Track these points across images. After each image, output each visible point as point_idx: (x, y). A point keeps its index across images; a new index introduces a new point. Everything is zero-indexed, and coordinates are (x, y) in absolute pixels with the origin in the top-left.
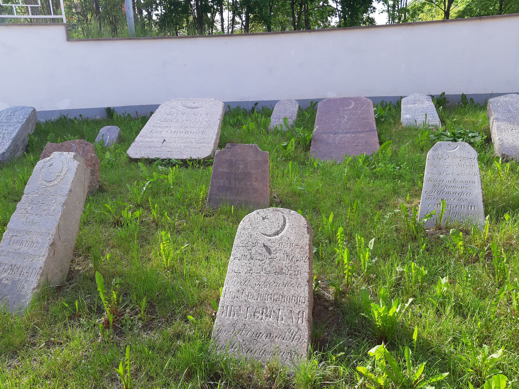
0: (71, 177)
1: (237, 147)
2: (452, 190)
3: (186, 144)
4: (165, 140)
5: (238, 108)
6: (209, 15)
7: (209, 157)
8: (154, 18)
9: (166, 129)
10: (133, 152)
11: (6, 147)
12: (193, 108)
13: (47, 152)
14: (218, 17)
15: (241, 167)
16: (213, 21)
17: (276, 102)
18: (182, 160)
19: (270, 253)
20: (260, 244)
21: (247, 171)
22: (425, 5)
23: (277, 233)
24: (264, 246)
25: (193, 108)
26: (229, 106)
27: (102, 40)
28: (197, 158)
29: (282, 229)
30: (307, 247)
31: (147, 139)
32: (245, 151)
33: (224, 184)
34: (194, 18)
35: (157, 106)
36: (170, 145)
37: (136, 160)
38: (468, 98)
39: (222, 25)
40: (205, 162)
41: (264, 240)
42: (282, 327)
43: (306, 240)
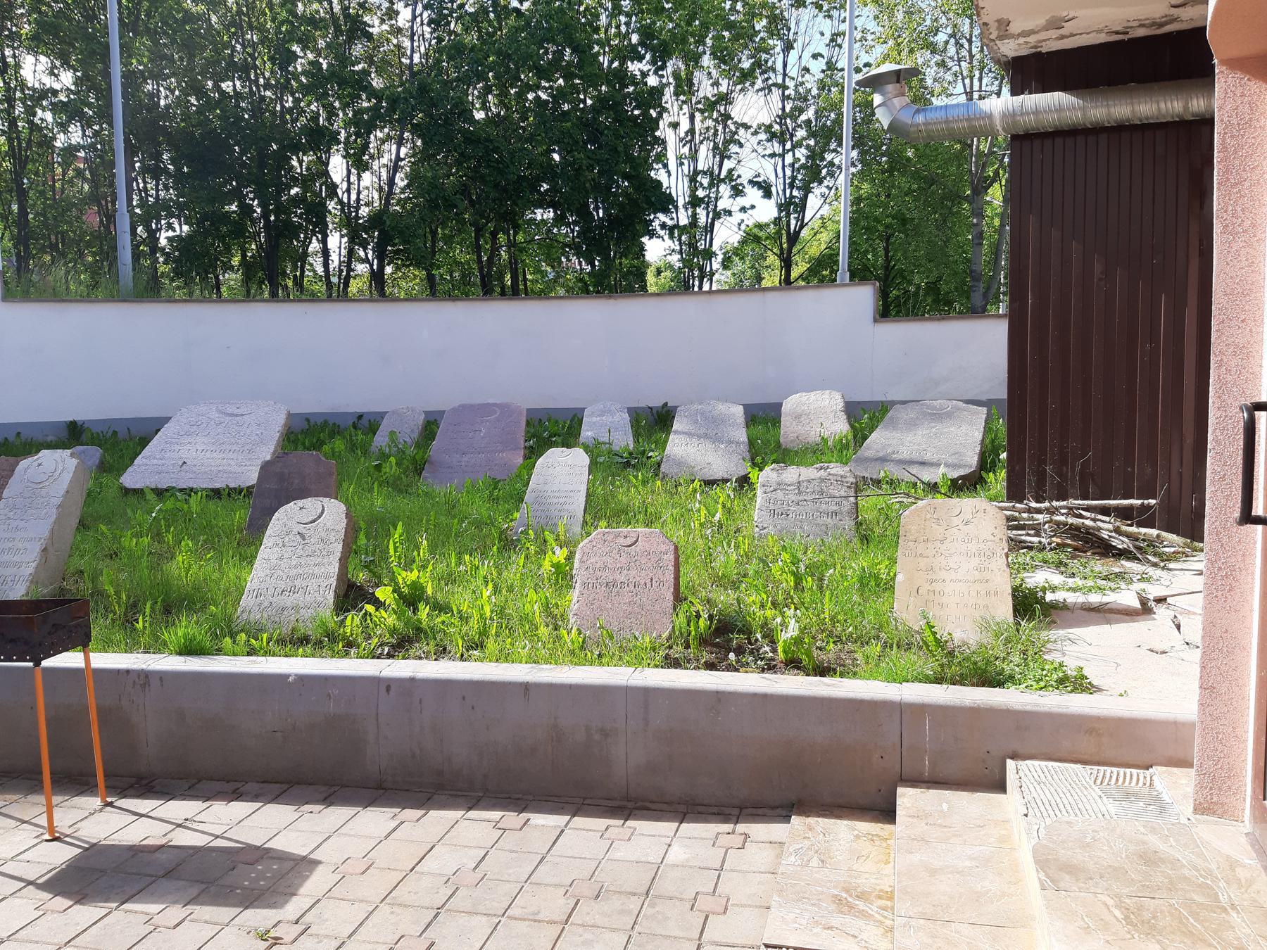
0: (67, 477)
1: (291, 455)
2: (555, 501)
3: (221, 468)
4: (185, 463)
5: (326, 422)
8: (163, 242)
9: (189, 447)
10: (130, 479)
12: (237, 415)
14: (315, 246)
15: (296, 481)
18: (212, 490)
19: (304, 540)
20: (295, 531)
24: (299, 533)
25: (237, 415)
26: (308, 420)
27: (71, 301)
28: (237, 486)
30: (344, 530)
31: (155, 462)
33: (271, 505)
34: (260, 247)
35: (167, 420)
36: (194, 469)
37: (138, 492)
39: (326, 265)
40: (249, 491)
41: (301, 528)
42: (308, 599)
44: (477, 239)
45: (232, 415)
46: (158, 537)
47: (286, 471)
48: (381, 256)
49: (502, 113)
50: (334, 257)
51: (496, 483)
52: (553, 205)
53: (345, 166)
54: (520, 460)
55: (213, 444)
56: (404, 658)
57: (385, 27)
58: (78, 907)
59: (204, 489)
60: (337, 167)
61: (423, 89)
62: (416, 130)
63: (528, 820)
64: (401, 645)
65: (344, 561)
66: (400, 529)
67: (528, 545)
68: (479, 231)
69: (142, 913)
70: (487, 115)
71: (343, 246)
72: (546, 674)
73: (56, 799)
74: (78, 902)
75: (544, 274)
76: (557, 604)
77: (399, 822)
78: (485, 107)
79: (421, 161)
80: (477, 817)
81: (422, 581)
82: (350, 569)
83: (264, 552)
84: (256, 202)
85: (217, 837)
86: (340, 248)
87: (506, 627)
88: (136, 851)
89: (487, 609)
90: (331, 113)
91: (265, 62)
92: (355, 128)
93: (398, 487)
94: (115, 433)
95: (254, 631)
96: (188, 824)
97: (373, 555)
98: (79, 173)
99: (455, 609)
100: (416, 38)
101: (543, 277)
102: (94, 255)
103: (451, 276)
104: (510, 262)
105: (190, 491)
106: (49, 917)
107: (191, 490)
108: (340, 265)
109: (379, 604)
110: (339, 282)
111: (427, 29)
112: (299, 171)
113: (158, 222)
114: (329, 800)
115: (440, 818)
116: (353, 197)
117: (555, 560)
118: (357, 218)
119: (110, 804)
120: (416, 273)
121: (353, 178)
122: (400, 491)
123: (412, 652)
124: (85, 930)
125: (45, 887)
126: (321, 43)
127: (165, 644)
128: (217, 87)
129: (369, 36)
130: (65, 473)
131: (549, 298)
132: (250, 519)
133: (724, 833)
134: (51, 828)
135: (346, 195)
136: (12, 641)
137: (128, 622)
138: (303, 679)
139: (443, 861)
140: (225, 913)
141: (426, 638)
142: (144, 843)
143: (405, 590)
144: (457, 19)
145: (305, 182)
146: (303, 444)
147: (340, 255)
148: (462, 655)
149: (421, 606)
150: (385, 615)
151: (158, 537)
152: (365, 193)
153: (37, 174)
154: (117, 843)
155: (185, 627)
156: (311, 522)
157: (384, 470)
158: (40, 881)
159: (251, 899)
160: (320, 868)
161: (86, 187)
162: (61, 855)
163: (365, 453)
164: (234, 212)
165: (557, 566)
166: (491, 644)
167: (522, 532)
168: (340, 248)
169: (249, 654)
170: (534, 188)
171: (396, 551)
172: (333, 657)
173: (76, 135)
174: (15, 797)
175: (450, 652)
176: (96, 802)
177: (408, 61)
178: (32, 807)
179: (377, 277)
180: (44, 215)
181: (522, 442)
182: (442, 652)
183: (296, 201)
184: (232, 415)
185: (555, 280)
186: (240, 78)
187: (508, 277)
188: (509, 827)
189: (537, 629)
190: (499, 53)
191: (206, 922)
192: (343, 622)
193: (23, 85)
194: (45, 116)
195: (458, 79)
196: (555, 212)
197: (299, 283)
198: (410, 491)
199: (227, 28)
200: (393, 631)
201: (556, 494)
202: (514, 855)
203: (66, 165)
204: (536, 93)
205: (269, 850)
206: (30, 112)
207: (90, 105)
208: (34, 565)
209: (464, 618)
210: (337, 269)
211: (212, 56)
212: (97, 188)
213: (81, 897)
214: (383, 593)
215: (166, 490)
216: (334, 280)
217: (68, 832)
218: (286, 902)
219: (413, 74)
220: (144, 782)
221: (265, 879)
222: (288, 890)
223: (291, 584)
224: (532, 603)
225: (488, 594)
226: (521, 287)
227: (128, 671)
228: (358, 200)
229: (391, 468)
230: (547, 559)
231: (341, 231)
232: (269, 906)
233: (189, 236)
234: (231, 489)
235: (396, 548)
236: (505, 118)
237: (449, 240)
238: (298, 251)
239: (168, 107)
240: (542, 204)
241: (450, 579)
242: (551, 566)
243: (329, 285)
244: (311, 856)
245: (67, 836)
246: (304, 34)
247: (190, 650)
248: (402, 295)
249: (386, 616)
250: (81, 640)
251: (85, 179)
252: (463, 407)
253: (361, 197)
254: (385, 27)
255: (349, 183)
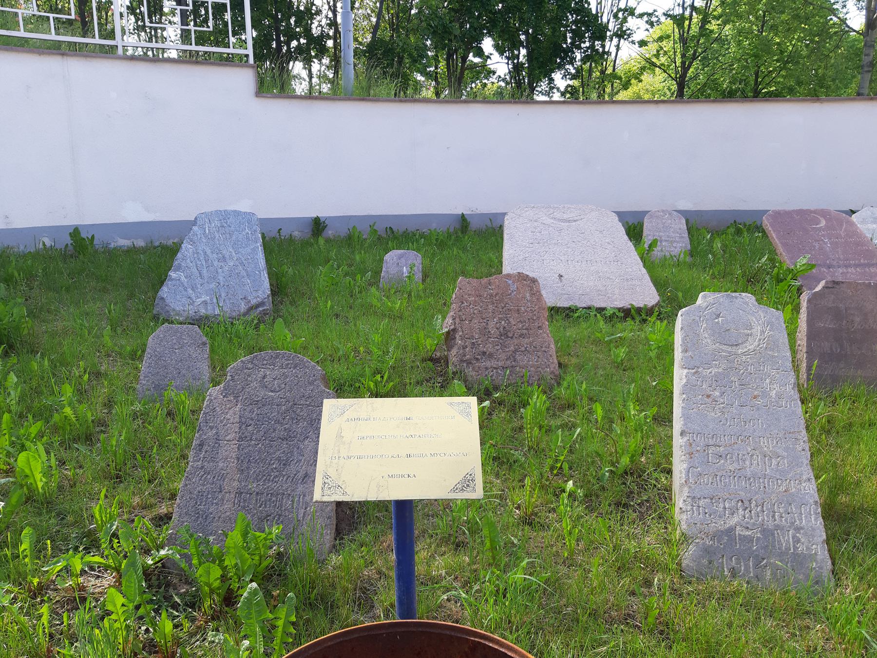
13: (463, 294)
15: (857, 319)
17: (646, 212)
21: (870, 326)
22: (644, 71)
32: (858, 293)
33: (831, 349)
38: (322, 220)
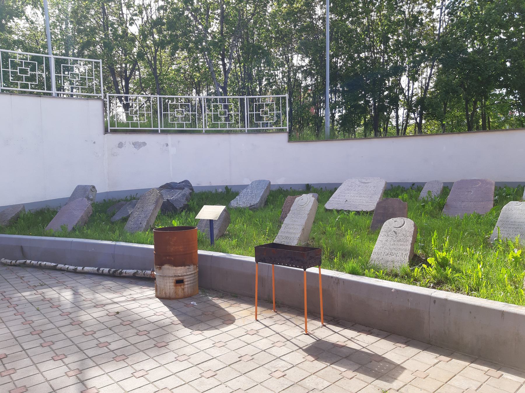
0: (311, 204)
3: (360, 203)
5: (399, 187)
6: (385, 113)
7: (373, 211)
9: (348, 195)
10: (328, 206)
11: (258, 201)
12: (366, 183)
14: (393, 114)
15: (391, 210)
16: (389, 118)
18: (357, 211)
19: (396, 234)
20: (393, 230)
23: (400, 227)
25: (366, 183)
26: (392, 185)
27: (309, 141)
29: (403, 225)
31: (336, 200)
34: (371, 116)
35: (340, 184)
37: (331, 211)
39: (397, 121)
40: (371, 213)
42: (398, 259)
43: (413, 229)
44: (466, 105)
45: (363, 183)
46: (339, 228)
47: (387, 206)
48: (421, 115)
49: (481, 48)
50: (401, 120)
51: (479, 216)
52: (506, 87)
53: (407, 80)
54: (492, 206)
55: (357, 194)
56: (440, 289)
57: (428, 20)
58: (316, 361)
59: (354, 211)
60: (404, 80)
61: (444, 43)
62: (441, 61)
63: (502, 375)
64: (438, 284)
65: (412, 244)
66: (435, 234)
67: (499, 246)
68: (467, 102)
69: (338, 370)
70: (473, 49)
71: (404, 113)
72: (514, 309)
73: (308, 320)
74: (316, 359)
75: (499, 118)
76: (516, 276)
77: (439, 360)
78: (473, 46)
79: (442, 74)
80: (476, 367)
81: (447, 257)
82: (415, 249)
83: (380, 238)
84: (371, 99)
85: (364, 347)
86: (403, 114)
87: (490, 284)
88: (335, 346)
89: (480, 274)
90: (403, 59)
91: (377, 43)
92: (413, 64)
93: (432, 215)
94: (321, 188)
95: (377, 269)
96: (352, 340)
97: (424, 243)
98: (309, 94)
99: (464, 272)
100: (442, 22)
101: (499, 120)
102: (312, 124)
103: (452, 122)
104: (482, 114)
105: (349, 212)
106: (307, 362)
107: (349, 211)
108: (403, 121)
109: (429, 265)
110: (402, 129)
111: (446, 17)
112: (388, 85)
113: (335, 110)
114: (408, 343)
115: (457, 364)
116: (410, 92)
117: (515, 255)
118: (412, 101)
119: (324, 326)
120: (436, 122)
121: (411, 85)
122: (433, 217)
123: (444, 288)
124: (319, 371)
125: (306, 351)
126: (400, 31)
127: (344, 268)
128: (359, 56)
129: (421, 24)
130: (310, 203)
131: (503, 130)
132: (372, 224)
133: (394, 390)
134: (306, 330)
135: (407, 92)
136: (298, 260)
137: (331, 259)
138: (398, 291)
139: (458, 382)
140: (369, 379)
141: (451, 282)
142: (337, 343)
143: (440, 260)
144: (461, 11)
145: (390, 89)
146: (390, 195)
147: (403, 117)
148: (468, 293)
149: (447, 268)
150: (431, 270)
151: (339, 228)
152: (415, 90)
153: (296, 96)
154: (328, 341)
155: (352, 263)
156: (399, 227)
157: (426, 207)
158: (304, 348)
159: (378, 376)
160: (406, 371)
161: (311, 99)
162: (309, 341)
163: (417, 199)
164: (363, 104)
165: (516, 258)
166: (483, 290)
167: (496, 240)
168: (403, 114)
169: (376, 278)
170: (497, 79)
171: (434, 243)
172: (410, 284)
173: (309, 81)
174: (294, 316)
175: (462, 291)
176: (320, 324)
177: (438, 32)
178: (300, 320)
179: (419, 125)
180: (297, 111)
181: (492, 198)
182: (458, 290)
183: (387, 97)
184: (363, 183)
185: (505, 121)
186: (367, 51)
187: (481, 121)
188: (492, 376)
189: (506, 287)
190: (481, 22)
191: (362, 380)
192: (413, 270)
193: (293, 65)
194: (300, 76)
195: (461, 36)
196: (507, 90)
197: (385, 130)
198: (437, 217)
199: (364, 32)
200: (434, 277)
201: (513, 223)
202: (496, 389)
203: (305, 92)
204: (499, 36)
205: (384, 358)
206: (295, 74)
207: (314, 70)
208: (300, 234)
209: (469, 277)
210: (401, 123)
211: (358, 44)
212: (315, 100)
213: (318, 358)
214: (430, 260)
215: (340, 210)
216: (400, 128)
217: (311, 333)
218: (393, 381)
219: (439, 37)
220: (336, 320)
221: (384, 369)
222: (393, 377)
223: (391, 251)
224: (504, 274)
225: (480, 267)
226: (487, 125)
227: (332, 277)
228: (412, 93)
229: (429, 206)
230: (510, 254)
231: (404, 107)
232: (386, 381)
233: (345, 114)
234: (363, 212)
235: (434, 241)
236: (483, 50)
237: (452, 107)
238: (386, 117)
239: (341, 67)
240: (500, 87)
241: (459, 258)
242: (512, 258)
243: (398, 130)
244: (402, 365)
245: (311, 334)
246: (393, 29)
247: (353, 272)
248: (429, 132)
249: (432, 270)
250: (318, 263)
251: (311, 97)
252: (462, 181)
253: (414, 92)
254: (428, 20)
255: (409, 87)
